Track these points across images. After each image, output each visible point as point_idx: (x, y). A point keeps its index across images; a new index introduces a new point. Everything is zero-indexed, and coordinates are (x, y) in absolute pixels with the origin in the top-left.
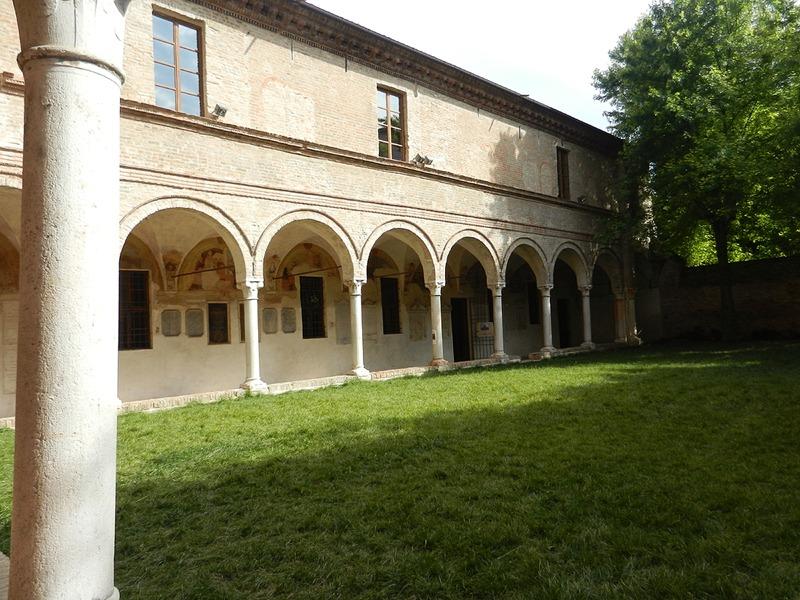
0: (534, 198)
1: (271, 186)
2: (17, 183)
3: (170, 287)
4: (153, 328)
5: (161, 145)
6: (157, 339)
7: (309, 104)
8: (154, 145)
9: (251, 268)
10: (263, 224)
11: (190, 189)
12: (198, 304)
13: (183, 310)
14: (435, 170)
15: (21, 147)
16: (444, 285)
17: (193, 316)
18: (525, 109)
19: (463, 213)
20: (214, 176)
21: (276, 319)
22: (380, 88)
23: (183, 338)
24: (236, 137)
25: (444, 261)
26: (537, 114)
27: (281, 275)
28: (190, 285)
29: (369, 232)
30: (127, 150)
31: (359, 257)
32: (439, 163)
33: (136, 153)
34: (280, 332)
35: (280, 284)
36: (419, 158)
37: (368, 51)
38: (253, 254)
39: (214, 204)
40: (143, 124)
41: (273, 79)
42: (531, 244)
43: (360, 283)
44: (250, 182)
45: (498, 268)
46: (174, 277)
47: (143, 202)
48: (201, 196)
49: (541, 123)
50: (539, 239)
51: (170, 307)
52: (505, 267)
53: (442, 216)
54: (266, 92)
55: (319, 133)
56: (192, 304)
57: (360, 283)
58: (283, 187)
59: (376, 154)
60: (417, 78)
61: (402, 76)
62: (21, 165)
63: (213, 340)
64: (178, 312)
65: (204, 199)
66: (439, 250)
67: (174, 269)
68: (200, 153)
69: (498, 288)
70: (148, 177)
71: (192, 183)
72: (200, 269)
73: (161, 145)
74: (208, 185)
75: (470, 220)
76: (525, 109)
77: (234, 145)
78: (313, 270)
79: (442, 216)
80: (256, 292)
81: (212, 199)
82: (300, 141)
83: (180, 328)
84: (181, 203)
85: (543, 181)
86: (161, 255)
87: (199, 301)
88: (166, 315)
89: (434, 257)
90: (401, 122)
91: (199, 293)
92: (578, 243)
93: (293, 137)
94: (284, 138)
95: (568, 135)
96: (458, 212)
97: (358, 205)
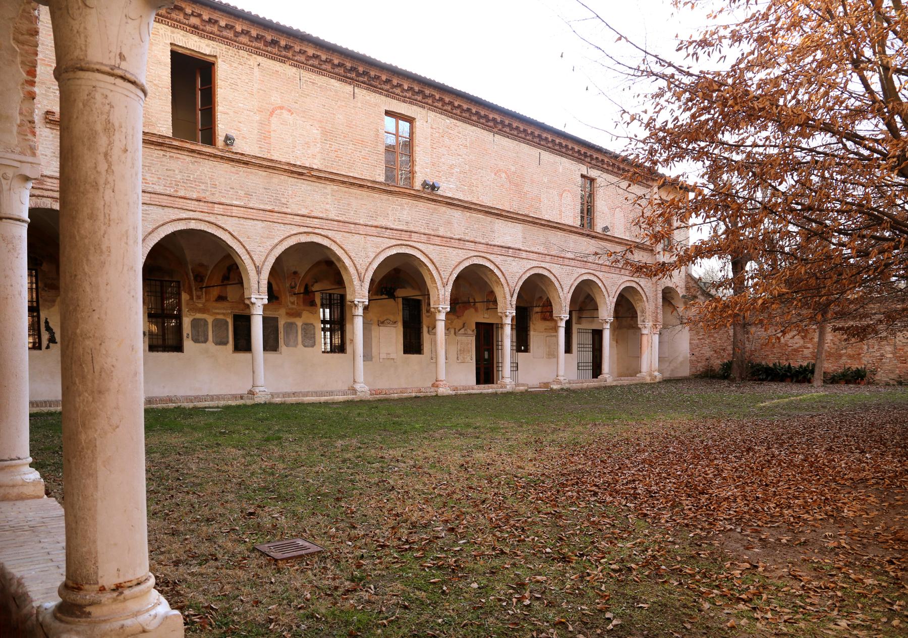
0: (551, 227)
1: (276, 209)
2: (56, 206)
3: (199, 297)
4: (185, 335)
5: (177, 172)
6: (188, 344)
7: (316, 132)
8: (172, 172)
9: (256, 286)
10: (269, 244)
11: (202, 212)
12: (224, 314)
13: (210, 319)
14: (442, 196)
15: (58, 175)
16: (514, 314)
17: (220, 325)
18: (544, 135)
19: (472, 239)
20: (223, 200)
21: (297, 333)
22: (388, 113)
23: (210, 345)
24: (244, 163)
25: (449, 288)
26: (557, 141)
27: (302, 291)
28: (217, 296)
29: (373, 256)
30: (148, 176)
31: (361, 280)
32: (447, 189)
33: (155, 180)
34: (300, 346)
35: (301, 300)
36: (425, 184)
37: (377, 78)
38: (259, 272)
39: (223, 225)
40: (162, 153)
41: (281, 108)
42: (546, 273)
43: (361, 305)
44: (257, 206)
45: (508, 297)
46: (201, 288)
47: (161, 223)
48: (212, 219)
49: (564, 150)
50: (556, 269)
51: (199, 316)
52: (515, 296)
53: (447, 241)
54: (274, 120)
55: (324, 159)
56: (218, 314)
57: (444, 311)
58: (289, 211)
59: (382, 179)
60: (427, 104)
61: (412, 101)
62: (58, 189)
63: (238, 348)
64: (206, 321)
65: (214, 221)
66: (445, 275)
67: (202, 281)
68: (211, 179)
69: (562, 319)
70: (165, 201)
71: (202, 206)
72: (225, 282)
73: (177, 172)
74: (218, 209)
75: (481, 247)
76: (544, 135)
77: (242, 169)
78: (334, 287)
79: (447, 241)
80: (444, 314)
81: (221, 221)
82: (305, 168)
83: (208, 335)
84: (193, 225)
85: (563, 209)
86: (190, 267)
87: (224, 311)
88: (195, 323)
89: (439, 283)
90: (409, 145)
91: (226, 304)
92: (636, 279)
93: (298, 163)
94: (289, 164)
95: (593, 162)
96: (467, 238)
97: (362, 230)
